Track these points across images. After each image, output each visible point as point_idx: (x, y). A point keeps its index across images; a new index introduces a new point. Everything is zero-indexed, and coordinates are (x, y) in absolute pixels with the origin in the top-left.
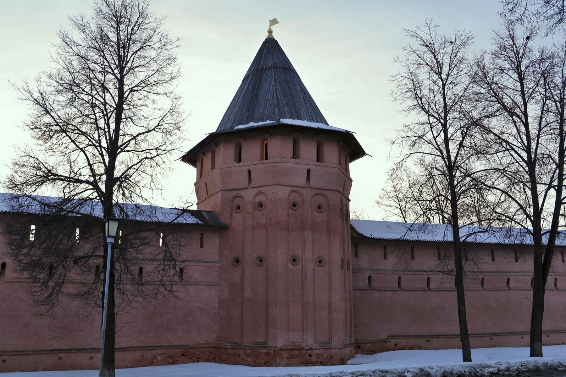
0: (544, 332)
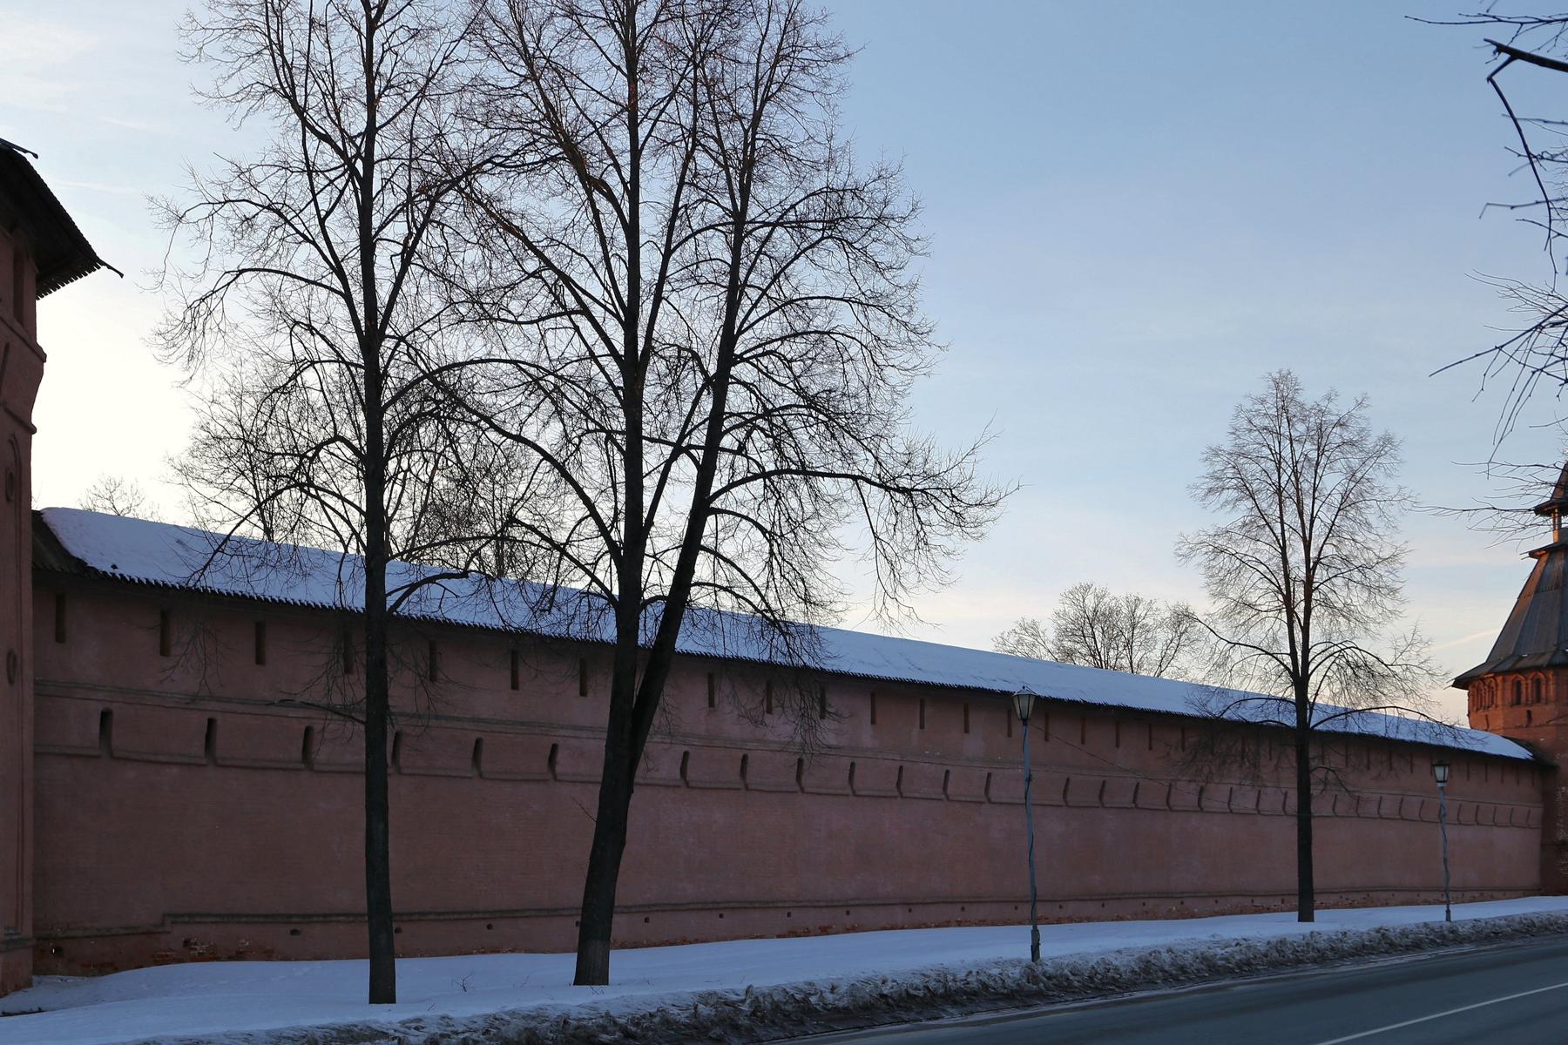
0: (619, 910)
